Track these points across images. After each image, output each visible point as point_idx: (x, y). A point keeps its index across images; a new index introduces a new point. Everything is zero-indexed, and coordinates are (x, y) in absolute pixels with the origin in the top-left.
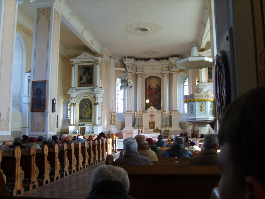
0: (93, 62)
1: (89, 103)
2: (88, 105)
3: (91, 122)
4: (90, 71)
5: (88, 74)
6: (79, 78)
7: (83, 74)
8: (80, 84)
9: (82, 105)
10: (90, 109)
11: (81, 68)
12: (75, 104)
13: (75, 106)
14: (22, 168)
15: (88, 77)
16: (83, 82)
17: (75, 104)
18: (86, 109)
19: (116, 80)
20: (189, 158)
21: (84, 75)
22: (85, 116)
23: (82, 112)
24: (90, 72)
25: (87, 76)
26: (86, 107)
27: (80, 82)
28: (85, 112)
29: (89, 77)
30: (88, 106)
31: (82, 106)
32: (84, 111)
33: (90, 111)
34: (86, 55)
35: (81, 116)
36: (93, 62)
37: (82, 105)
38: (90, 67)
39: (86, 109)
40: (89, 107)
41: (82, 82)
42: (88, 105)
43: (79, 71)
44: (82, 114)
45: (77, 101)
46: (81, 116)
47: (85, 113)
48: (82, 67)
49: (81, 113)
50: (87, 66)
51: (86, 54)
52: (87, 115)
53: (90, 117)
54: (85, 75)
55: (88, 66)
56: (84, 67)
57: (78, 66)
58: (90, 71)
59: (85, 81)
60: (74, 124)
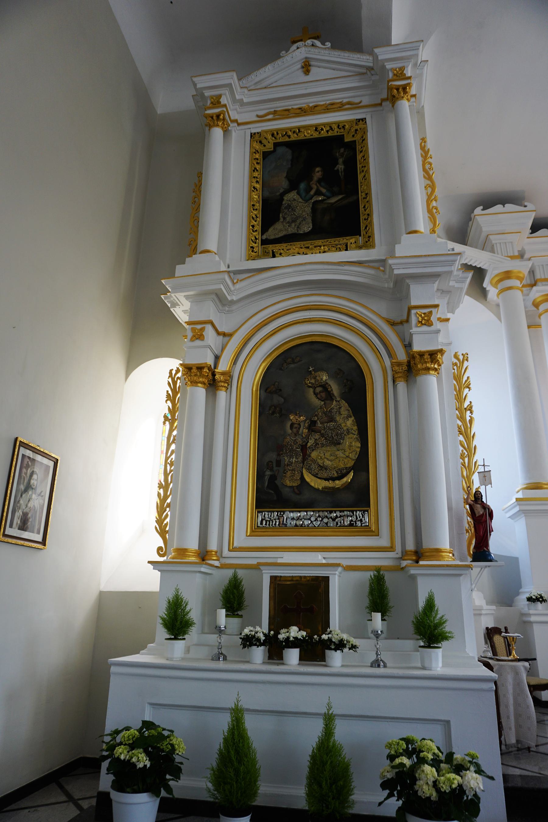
0: (354, 106)
1: (336, 375)
2: (335, 389)
3: (367, 531)
4: (341, 160)
5: (319, 181)
6: (259, 206)
7: (285, 184)
8: (264, 242)
9: (278, 391)
10: (350, 423)
11: (274, 151)
12: (228, 375)
13: (222, 395)
14: (141, 768)
15: (329, 198)
16: (292, 230)
17: (228, 375)
18: (313, 423)
19: (361, 448)
20: (164, 789)
21: (293, 186)
22: (308, 478)
23: (280, 449)
24: (340, 167)
25: (318, 193)
26: (316, 402)
27: (262, 234)
28: (304, 448)
29: (334, 194)
30: (330, 396)
31: (277, 399)
32: (299, 440)
33: (355, 434)
34: (306, 67)
35: (273, 478)
36: (354, 106)
37: (278, 391)
38: (341, 138)
39: (313, 423)
40: (344, 404)
41: (271, 233)
42: (335, 389)
43: (258, 167)
44: (278, 463)
45: (305, 89)
46: (273, 478)
47: (305, 456)
48: (276, 145)
49: (272, 456)
50: (316, 135)
51: (313, 54)
52: (323, 468)
53: (348, 487)
54: (302, 186)
55: (324, 134)
56: (290, 145)
57: (252, 135)
58: (341, 160)
59: (307, 228)
60: (213, 546)
